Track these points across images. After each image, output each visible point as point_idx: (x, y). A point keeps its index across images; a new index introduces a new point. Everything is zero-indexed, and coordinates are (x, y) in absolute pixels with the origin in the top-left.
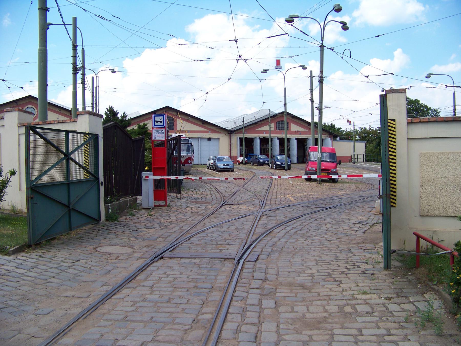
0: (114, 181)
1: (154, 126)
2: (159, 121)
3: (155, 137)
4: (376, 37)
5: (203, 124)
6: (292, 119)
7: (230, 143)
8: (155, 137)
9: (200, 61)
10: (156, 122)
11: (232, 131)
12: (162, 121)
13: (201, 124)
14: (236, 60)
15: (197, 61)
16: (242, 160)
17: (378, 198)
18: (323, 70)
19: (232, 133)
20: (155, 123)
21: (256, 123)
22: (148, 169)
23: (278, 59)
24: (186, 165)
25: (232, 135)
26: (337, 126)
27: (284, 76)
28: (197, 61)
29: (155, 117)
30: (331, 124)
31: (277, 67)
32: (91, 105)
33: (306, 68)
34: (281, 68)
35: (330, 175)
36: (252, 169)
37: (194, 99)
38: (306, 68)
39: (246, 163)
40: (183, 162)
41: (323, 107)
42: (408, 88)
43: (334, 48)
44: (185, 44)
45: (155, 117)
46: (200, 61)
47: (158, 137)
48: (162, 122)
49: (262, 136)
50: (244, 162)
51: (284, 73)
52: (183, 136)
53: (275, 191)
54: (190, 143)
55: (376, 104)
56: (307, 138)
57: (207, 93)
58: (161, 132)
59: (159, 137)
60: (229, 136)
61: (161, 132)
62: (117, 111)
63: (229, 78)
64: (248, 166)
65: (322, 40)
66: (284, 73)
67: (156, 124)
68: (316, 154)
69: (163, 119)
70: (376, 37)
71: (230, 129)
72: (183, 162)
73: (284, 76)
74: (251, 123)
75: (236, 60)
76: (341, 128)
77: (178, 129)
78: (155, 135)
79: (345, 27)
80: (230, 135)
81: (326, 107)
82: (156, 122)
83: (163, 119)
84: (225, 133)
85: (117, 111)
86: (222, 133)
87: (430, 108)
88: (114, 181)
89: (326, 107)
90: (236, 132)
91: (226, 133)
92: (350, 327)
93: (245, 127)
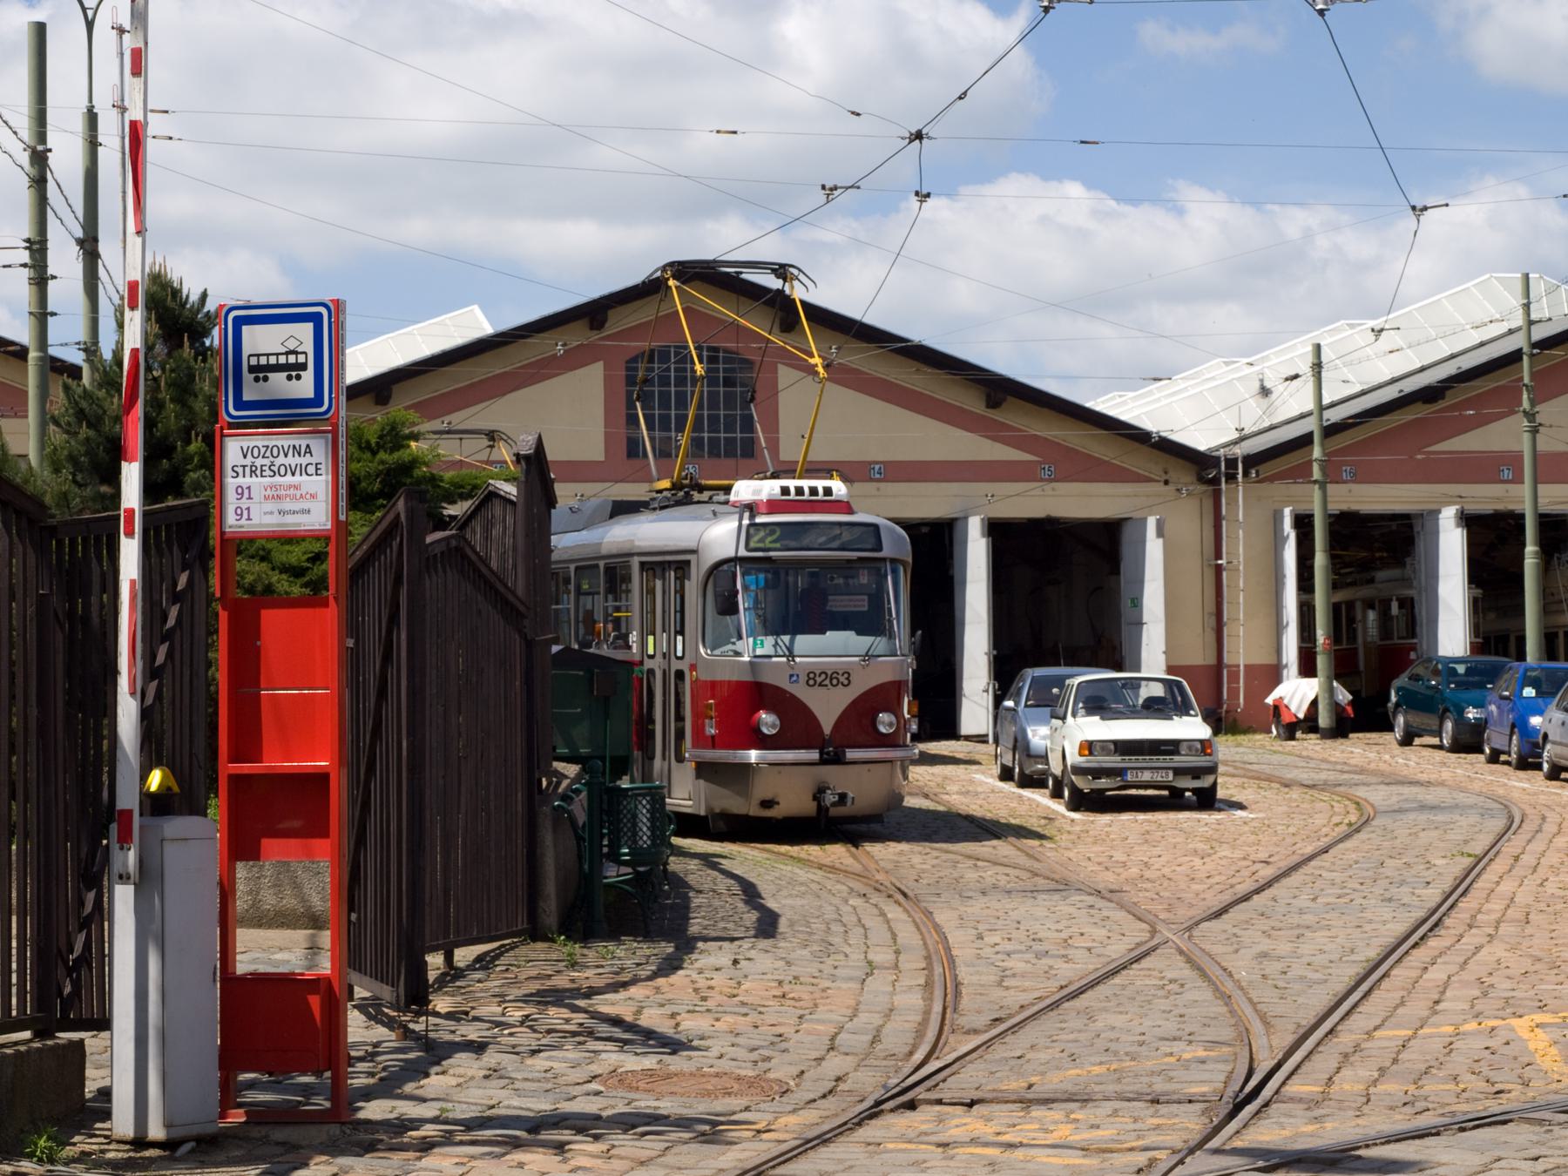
3: (244, 503)
5: (993, 404)
7: (1218, 555)
8: (244, 503)
11: (1231, 463)
12: (303, 367)
13: (972, 402)
16: (1314, 703)
17: (670, 966)
19: (1231, 478)
20: (248, 377)
21: (1429, 395)
22: (165, 788)
24: (851, 754)
25: (1233, 501)
32: (25, 256)
36: (1374, 773)
39: (1342, 728)
40: (827, 728)
47: (269, 506)
48: (308, 376)
49: (1488, 497)
50: (1324, 720)
52: (828, 491)
53: (1437, 974)
54: (893, 561)
55: (821, 197)
58: (292, 460)
60: (1208, 504)
61: (292, 460)
62: (204, 296)
64: (1360, 750)
68: (864, 600)
69: (309, 347)
71: (1217, 449)
72: (827, 728)
74: (1390, 394)
77: (790, 450)
78: (240, 492)
80: (1217, 496)
82: (252, 369)
84: (1172, 476)
85: (204, 296)
86: (1149, 480)
90: (1268, 469)
91: (1184, 476)
93: (1331, 431)
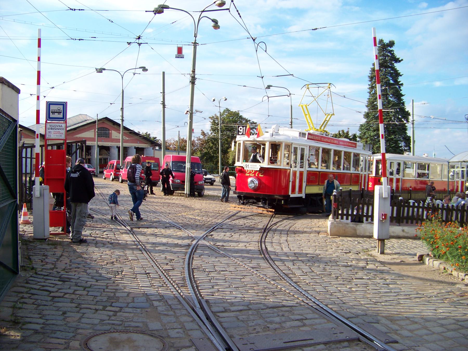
0: (18, 194)
1: (49, 118)
2: (56, 112)
4: (313, 30)
6: (113, 126)
9: (79, 40)
10: (52, 112)
12: (61, 112)
14: (128, 43)
15: (75, 39)
18: (195, 70)
20: (51, 114)
23: (179, 46)
26: (152, 136)
27: (122, 78)
28: (75, 39)
29: (51, 105)
30: (146, 134)
31: (178, 56)
33: (147, 70)
34: (183, 57)
35: (400, 190)
37: (31, 95)
38: (147, 70)
41: (194, 111)
42: (288, 95)
43: (256, 38)
44: (79, 10)
45: (51, 105)
46: (79, 40)
48: (62, 114)
51: (122, 74)
56: (128, 146)
57: (53, 88)
59: (55, 135)
63: (251, 45)
65: (195, 36)
66: (122, 74)
67: (52, 116)
70: (313, 30)
73: (122, 78)
75: (128, 43)
76: (156, 138)
78: (49, 132)
79: (216, 25)
81: (197, 111)
82: (52, 112)
83: (62, 109)
87: (250, 120)
88: (18, 194)
89: (197, 111)
92: (59, 301)
